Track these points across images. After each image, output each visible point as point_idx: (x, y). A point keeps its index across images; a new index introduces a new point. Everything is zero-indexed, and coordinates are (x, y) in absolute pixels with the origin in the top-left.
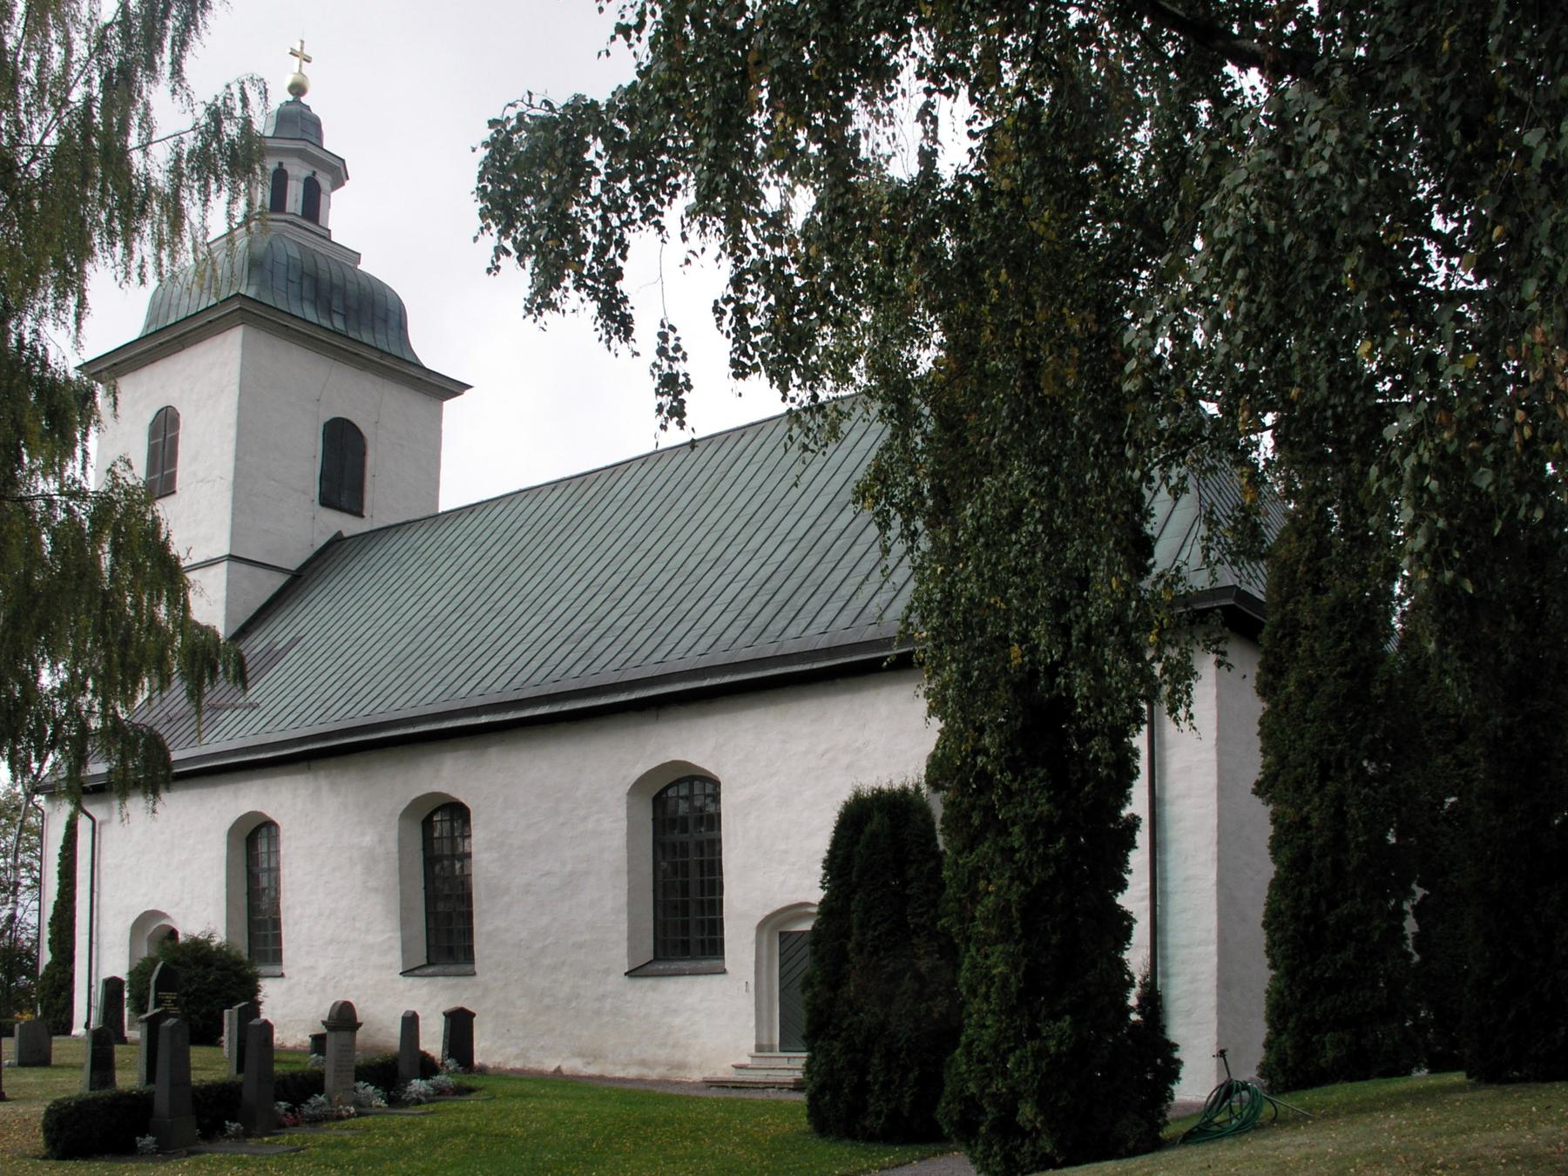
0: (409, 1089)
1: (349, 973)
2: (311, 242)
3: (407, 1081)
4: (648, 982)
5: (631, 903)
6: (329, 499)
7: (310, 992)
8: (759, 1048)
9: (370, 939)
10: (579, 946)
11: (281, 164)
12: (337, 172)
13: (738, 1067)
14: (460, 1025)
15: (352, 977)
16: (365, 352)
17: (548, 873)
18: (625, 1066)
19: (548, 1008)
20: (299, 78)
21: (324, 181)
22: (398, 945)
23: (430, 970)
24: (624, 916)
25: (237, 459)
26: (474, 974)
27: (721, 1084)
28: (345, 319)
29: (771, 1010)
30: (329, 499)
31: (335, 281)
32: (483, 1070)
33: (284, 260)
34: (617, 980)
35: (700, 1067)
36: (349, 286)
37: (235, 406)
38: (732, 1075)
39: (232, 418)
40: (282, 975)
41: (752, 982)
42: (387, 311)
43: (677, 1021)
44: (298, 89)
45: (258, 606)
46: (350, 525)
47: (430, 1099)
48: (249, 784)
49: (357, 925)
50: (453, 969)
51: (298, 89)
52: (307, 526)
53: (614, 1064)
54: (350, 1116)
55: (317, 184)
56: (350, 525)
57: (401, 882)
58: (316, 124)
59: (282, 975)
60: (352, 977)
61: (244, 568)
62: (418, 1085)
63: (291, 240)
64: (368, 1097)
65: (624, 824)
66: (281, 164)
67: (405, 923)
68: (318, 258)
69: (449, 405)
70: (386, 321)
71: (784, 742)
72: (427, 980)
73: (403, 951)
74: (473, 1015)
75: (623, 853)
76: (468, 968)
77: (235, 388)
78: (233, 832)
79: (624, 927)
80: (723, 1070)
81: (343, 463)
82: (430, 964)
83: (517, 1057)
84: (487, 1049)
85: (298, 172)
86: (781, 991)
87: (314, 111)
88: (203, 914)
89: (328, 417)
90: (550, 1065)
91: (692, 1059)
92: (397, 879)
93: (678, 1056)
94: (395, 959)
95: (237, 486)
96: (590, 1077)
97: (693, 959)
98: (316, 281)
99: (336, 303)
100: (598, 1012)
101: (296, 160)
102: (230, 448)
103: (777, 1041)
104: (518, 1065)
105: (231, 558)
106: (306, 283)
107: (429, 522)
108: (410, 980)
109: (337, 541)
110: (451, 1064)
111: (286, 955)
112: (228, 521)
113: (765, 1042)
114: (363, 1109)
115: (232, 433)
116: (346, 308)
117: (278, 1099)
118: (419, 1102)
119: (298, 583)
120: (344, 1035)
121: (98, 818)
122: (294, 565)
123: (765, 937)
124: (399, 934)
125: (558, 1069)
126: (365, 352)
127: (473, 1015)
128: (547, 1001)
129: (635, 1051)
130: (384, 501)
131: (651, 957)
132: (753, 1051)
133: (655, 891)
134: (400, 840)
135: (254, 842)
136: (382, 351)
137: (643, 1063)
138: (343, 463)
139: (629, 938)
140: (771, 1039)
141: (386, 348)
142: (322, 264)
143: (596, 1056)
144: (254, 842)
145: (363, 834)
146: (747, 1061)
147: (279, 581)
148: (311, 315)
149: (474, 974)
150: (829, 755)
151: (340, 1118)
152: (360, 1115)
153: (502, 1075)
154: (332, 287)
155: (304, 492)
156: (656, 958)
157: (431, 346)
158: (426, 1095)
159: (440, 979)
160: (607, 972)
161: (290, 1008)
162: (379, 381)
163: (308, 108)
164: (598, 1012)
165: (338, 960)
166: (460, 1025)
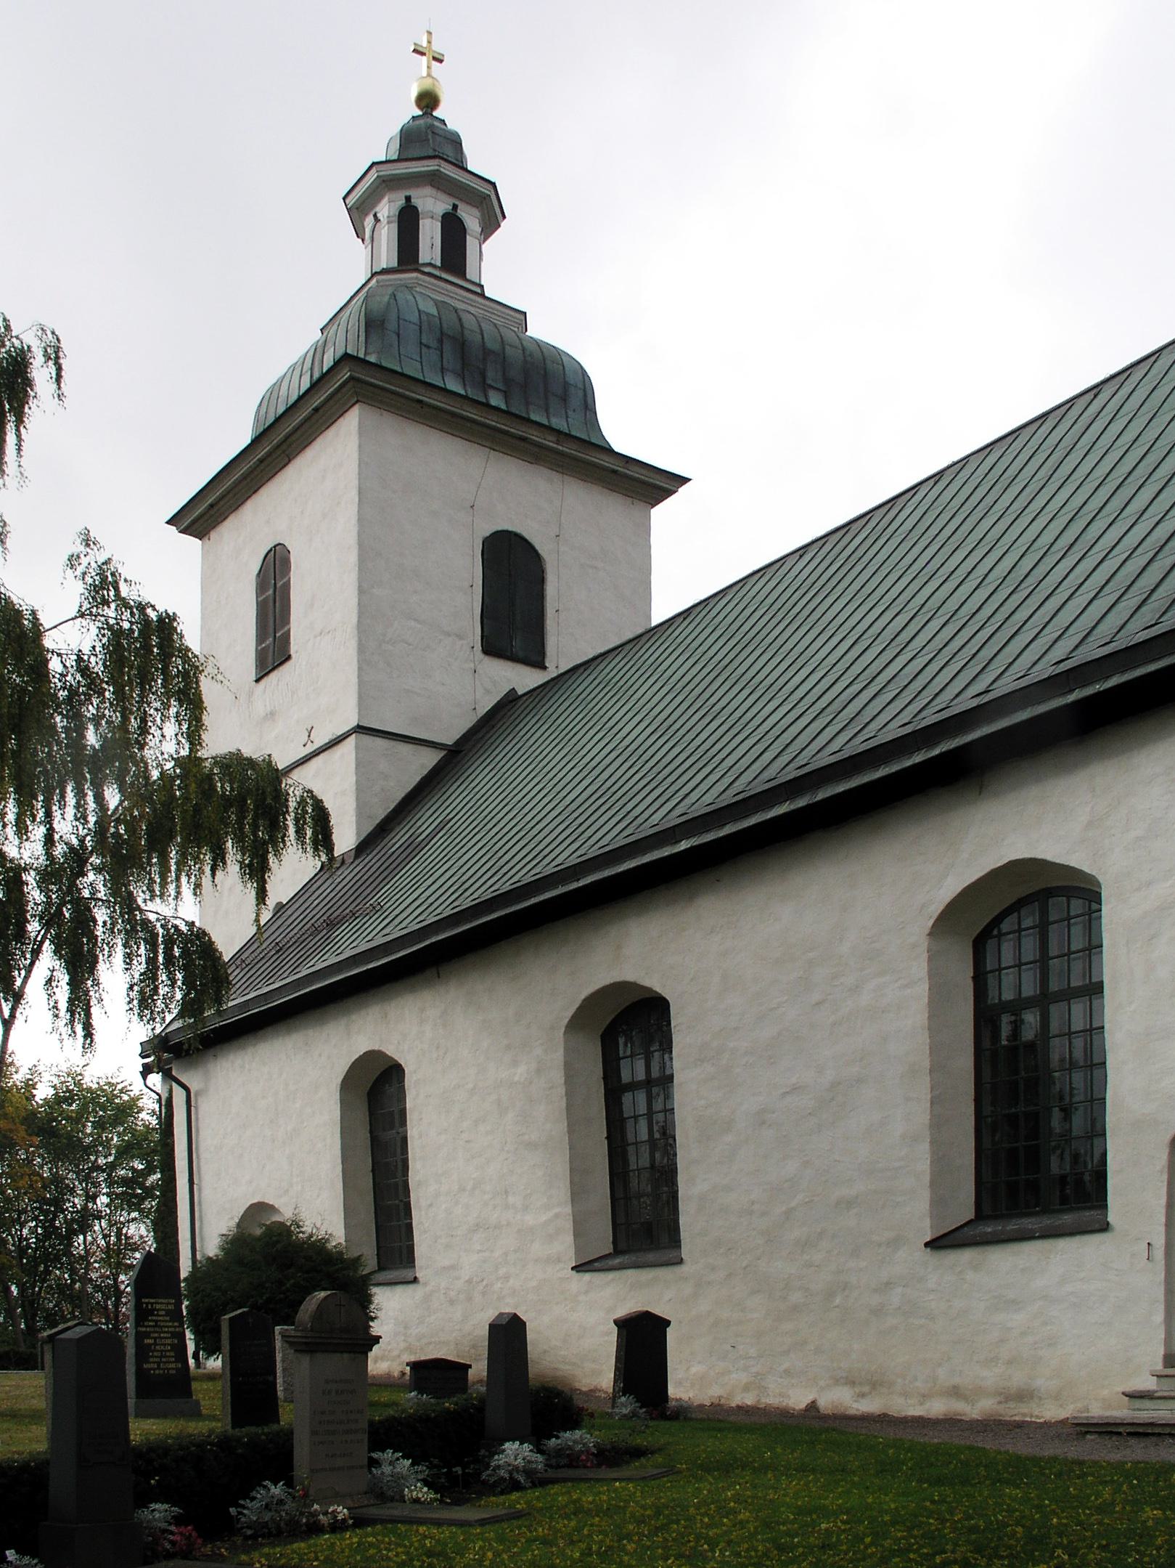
0: (499, 1460)
1: (502, 1271)
2: (458, 300)
3: (495, 1446)
4: (967, 1255)
5: (938, 1123)
6: (492, 647)
7: (452, 1302)
9: (530, 1219)
10: (849, 1203)
11: (408, 199)
12: (492, 217)
13: (1132, 1396)
14: (642, 1340)
15: (507, 1278)
16: (535, 435)
17: (795, 1089)
18: (925, 1397)
19: (795, 1309)
20: (427, 84)
21: (471, 220)
22: (569, 1225)
23: (617, 1261)
24: (924, 1148)
25: (361, 591)
26: (681, 1262)
27: (1108, 1430)
28: (506, 396)
30: (492, 647)
31: (489, 345)
32: (682, 1414)
33: (414, 318)
34: (913, 1255)
35: (1057, 1397)
36: (508, 350)
37: (354, 520)
38: (1122, 1412)
39: (351, 539)
40: (415, 1280)
42: (566, 385)
44: (428, 100)
45: (400, 794)
46: (525, 679)
47: (538, 1481)
48: (363, 1013)
49: (511, 1199)
50: (651, 1257)
51: (428, 100)
52: (467, 683)
53: (905, 1395)
54: (337, 1527)
55: (460, 223)
56: (525, 679)
57: (571, 1130)
58: (455, 141)
59: (415, 1280)
60: (507, 1278)
61: (380, 742)
62: (515, 1453)
63: (427, 295)
64: (397, 1478)
65: (923, 989)
66: (408, 199)
67: (577, 1193)
68: (464, 316)
69: (661, 514)
70: (564, 399)
72: (611, 1275)
73: (577, 1235)
74: (668, 1323)
75: (924, 1039)
76: (671, 1254)
77: (353, 495)
78: (349, 1083)
79: (923, 1166)
80: (1102, 1400)
81: (512, 589)
82: (617, 1251)
83: (746, 1388)
84: (691, 1376)
85: (432, 205)
87: (451, 125)
88: (320, 1206)
90: (798, 1399)
91: (1042, 1383)
92: (563, 1126)
93: (1018, 1378)
94: (565, 1247)
95: (363, 629)
96: (865, 1419)
97: (1045, 1211)
98: (461, 345)
99: (492, 376)
100: (878, 1312)
101: (428, 190)
102: (351, 579)
104: (749, 1400)
105: (360, 729)
106: (447, 347)
107: (628, 647)
108: (587, 1277)
109: (510, 701)
110: (627, 1405)
112: (354, 680)
114: (376, 1507)
115: (353, 558)
116: (507, 381)
117: (143, 1499)
118: (515, 1486)
119: (455, 759)
120: (334, 1364)
121: (194, 1087)
122: (450, 738)
124: (568, 1209)
125: (813, 1406)
126: (535, 435)
127: (668, 1323)
128: (796, 1297)
129: (942, 1373)
130: (571, 636)
131: (970, 1214)
133: (978, 1101)
134: (568, 1066)
135: (376, 1095)
136: (559, 432)
137: (955, 1392)
138: (512, 589)
139: (933, 1184)
141: (564, 428)
142: (469, 321)
143: (876, 1384)
144: (376, 1095)
145: (515, 1063)
146: (1149, 1384)
147: (430, 759)
148: (453, 385)
149: (681, 1262)
151: (314, 1529)
152: (360, 1522)
153: (717, 1419)
154: (486, 352)
155: (460, 637)
156: (980, 1216)
157: (625, 427)
158: (529, 1473)
159: (630, 1272)
160: (895, 1243)
161: (409, 1325)
162: (556, 477)
163: (443, 122)
164: (878, 1312)
165: (495, 1254)
166: (642, 1340)
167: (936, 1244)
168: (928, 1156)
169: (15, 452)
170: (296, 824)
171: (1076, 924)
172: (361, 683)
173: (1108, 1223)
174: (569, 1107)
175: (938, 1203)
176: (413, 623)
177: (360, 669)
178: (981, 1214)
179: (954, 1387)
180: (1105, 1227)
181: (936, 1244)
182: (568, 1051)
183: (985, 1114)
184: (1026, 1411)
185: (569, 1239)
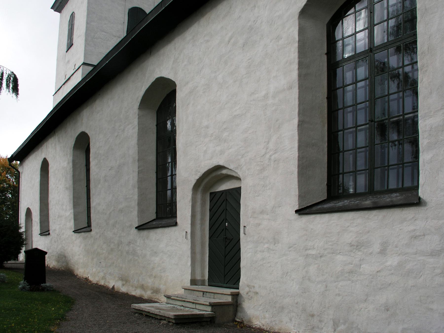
5: (141, 181)
8: (193, 282)
24: (136, 190)
25: (87, 23)
29: (203, 254)
34: (70, 232)
41: (189, 231)
43: (157, 259)
71: (208, 41)
73: (75, 220)
79: (136, 197)
86: (210, 238)
89: (130, 6)
94: (71, 224)
103: (207, 278)
111: (92, 225)
113: (198, 277)
123: (199, 196)
124: (72, 211)
131: (154, 217)
132: (187, 284)
134: (74, 162)
140: (203, 275)
143: (125, 280)
150: (232, 41)
167: (140, 228)
168: (137, 193)
169: (77, 16)
170: (7, 82)
171: (406, 166)
172: (85, 50)
173: (420, 198)
174: (74, 176)
175: (141, 212)
176: (104, 33)
177: (85, 46)
178: (158, 218)
179: (143, 285)
180: (176, 224)
181: (140, 228)
182: (74, 156)
183: (170, 177)
184: (157, 297)
185: (73, 221)
